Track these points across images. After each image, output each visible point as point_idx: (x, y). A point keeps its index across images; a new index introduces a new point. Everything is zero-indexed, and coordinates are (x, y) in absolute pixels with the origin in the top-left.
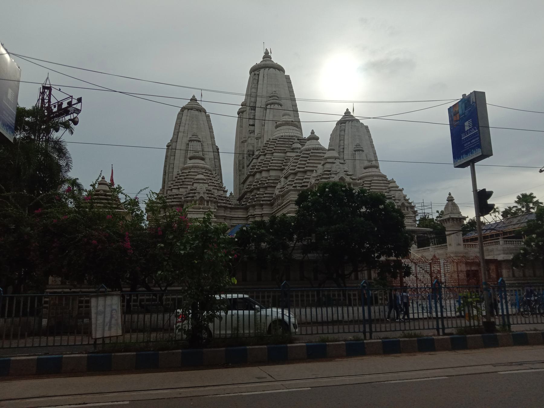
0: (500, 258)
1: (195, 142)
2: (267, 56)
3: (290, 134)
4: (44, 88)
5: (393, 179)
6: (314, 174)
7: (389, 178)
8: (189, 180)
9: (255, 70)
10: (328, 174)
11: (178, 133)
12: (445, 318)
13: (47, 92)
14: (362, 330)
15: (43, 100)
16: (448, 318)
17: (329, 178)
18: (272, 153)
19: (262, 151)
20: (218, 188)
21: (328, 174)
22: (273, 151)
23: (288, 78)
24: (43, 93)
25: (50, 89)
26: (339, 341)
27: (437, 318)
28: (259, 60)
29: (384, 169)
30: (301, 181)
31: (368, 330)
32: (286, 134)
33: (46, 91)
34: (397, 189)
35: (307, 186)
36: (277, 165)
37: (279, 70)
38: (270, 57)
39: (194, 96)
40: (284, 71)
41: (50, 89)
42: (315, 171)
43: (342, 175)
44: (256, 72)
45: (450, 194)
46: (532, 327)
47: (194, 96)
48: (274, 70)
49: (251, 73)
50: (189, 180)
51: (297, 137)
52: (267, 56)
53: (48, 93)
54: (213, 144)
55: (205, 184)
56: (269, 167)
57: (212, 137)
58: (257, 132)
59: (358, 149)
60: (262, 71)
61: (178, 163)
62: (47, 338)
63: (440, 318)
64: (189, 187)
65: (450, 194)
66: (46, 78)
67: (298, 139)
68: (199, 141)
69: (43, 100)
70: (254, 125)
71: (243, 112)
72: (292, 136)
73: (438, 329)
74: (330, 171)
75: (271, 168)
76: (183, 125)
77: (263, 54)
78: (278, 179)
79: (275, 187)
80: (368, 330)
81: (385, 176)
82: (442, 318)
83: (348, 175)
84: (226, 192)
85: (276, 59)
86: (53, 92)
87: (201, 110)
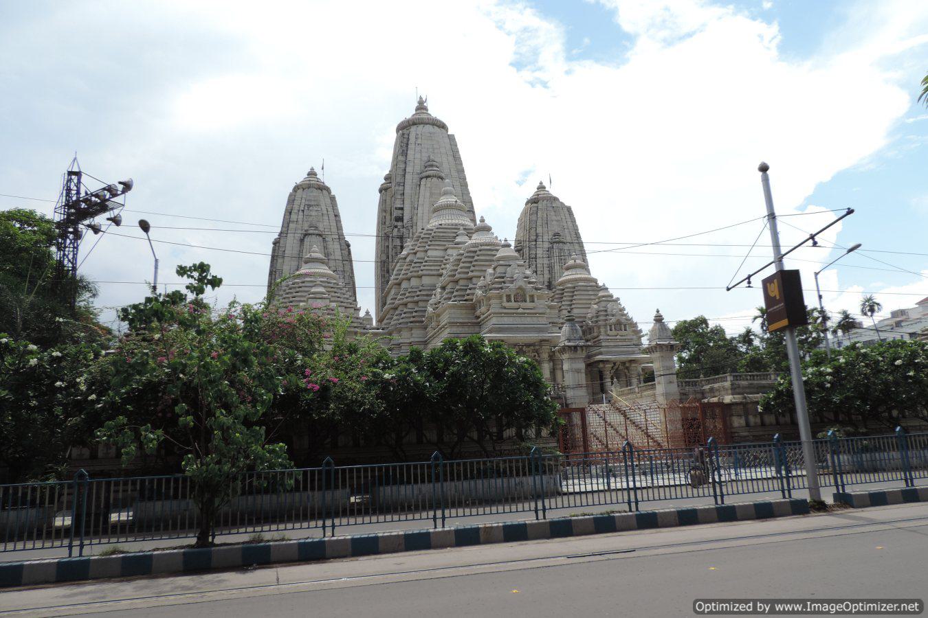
0: (728, 399)
1: (314, 236)
2: (421, 107)
3: (454, 221)
4: (70, 173)
5: (604, 285)
6: (481, 283)
7: (600, 284)
8: (303, 294)
9: (404, 128)
10: (500, 283)
11: (288, 224)
12: (639, 488)
13: (75, 178)
14: (533, 508)
15: (69, 190)
16: (642, 488)
17: (502, 288)
18: (426, 251)
19: (412, 248)
20: (345, 305)
21: (500, 283)
22: (427, 247)
23: (452, 138)
24: (70, 180)
25: (78, 174)
26: (290, 540)
27: (628, 489)
28: (409, 113)
29: (601, 269)
30: (462, 293)
31: (633, 498)
32: (447, 222)
33: (73, 177)
34: (609, 299)
35: (472, 300)
36: (433, 268)
37: (439, 127)
38: (426, 109)
39: (312, 169)
40: (447, 131)
41: (78, 174)
42: (482, 278)
43: (520, 283)
44: (405, 131)
45: (658, 311)
46: (580, 510)
47: (312, 169)
48: (431, 127)
49: (398, 130)
50: (303, 294)
51: (463, 225)
52: (421, 107)
53: (76, 181)
54: (341, 237)
55: (324, 300)
56: (420, 272)
57: (339, 228)
58: (406, 218)
59: (557, 240)
60: (413, 129)
61: (287, 267)
62: (6, 545)
63: (632, 489)
64: (302, 304)
65: (658, 311)
66: (73, 159)
67: (465, 229)
68: (320, 235)
69: (69, 190)
70: (402, 209)
71: (386, 189)
72: (456, 225)
73: (629, 503)
74: (503, 277)
75: (424, 272)
76: (296, 211)
77: (416, 104)
78: (433, 288)
79: (428, 301)
80: (633, 498)
81: (595, 281)
82: (635, 489)
83: (530, 283)
84: (359, 310)
85: (435, 111)
86: (84, 179)
87: (323, 188)
